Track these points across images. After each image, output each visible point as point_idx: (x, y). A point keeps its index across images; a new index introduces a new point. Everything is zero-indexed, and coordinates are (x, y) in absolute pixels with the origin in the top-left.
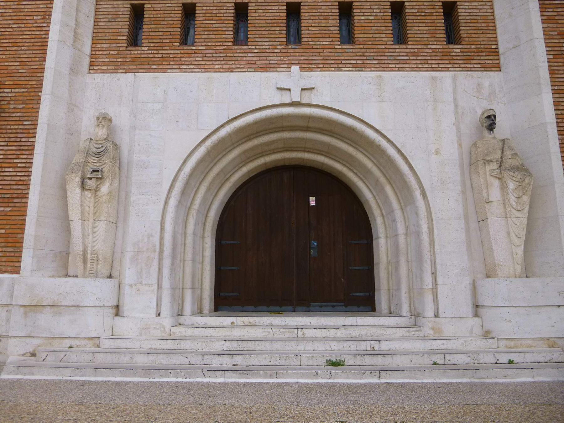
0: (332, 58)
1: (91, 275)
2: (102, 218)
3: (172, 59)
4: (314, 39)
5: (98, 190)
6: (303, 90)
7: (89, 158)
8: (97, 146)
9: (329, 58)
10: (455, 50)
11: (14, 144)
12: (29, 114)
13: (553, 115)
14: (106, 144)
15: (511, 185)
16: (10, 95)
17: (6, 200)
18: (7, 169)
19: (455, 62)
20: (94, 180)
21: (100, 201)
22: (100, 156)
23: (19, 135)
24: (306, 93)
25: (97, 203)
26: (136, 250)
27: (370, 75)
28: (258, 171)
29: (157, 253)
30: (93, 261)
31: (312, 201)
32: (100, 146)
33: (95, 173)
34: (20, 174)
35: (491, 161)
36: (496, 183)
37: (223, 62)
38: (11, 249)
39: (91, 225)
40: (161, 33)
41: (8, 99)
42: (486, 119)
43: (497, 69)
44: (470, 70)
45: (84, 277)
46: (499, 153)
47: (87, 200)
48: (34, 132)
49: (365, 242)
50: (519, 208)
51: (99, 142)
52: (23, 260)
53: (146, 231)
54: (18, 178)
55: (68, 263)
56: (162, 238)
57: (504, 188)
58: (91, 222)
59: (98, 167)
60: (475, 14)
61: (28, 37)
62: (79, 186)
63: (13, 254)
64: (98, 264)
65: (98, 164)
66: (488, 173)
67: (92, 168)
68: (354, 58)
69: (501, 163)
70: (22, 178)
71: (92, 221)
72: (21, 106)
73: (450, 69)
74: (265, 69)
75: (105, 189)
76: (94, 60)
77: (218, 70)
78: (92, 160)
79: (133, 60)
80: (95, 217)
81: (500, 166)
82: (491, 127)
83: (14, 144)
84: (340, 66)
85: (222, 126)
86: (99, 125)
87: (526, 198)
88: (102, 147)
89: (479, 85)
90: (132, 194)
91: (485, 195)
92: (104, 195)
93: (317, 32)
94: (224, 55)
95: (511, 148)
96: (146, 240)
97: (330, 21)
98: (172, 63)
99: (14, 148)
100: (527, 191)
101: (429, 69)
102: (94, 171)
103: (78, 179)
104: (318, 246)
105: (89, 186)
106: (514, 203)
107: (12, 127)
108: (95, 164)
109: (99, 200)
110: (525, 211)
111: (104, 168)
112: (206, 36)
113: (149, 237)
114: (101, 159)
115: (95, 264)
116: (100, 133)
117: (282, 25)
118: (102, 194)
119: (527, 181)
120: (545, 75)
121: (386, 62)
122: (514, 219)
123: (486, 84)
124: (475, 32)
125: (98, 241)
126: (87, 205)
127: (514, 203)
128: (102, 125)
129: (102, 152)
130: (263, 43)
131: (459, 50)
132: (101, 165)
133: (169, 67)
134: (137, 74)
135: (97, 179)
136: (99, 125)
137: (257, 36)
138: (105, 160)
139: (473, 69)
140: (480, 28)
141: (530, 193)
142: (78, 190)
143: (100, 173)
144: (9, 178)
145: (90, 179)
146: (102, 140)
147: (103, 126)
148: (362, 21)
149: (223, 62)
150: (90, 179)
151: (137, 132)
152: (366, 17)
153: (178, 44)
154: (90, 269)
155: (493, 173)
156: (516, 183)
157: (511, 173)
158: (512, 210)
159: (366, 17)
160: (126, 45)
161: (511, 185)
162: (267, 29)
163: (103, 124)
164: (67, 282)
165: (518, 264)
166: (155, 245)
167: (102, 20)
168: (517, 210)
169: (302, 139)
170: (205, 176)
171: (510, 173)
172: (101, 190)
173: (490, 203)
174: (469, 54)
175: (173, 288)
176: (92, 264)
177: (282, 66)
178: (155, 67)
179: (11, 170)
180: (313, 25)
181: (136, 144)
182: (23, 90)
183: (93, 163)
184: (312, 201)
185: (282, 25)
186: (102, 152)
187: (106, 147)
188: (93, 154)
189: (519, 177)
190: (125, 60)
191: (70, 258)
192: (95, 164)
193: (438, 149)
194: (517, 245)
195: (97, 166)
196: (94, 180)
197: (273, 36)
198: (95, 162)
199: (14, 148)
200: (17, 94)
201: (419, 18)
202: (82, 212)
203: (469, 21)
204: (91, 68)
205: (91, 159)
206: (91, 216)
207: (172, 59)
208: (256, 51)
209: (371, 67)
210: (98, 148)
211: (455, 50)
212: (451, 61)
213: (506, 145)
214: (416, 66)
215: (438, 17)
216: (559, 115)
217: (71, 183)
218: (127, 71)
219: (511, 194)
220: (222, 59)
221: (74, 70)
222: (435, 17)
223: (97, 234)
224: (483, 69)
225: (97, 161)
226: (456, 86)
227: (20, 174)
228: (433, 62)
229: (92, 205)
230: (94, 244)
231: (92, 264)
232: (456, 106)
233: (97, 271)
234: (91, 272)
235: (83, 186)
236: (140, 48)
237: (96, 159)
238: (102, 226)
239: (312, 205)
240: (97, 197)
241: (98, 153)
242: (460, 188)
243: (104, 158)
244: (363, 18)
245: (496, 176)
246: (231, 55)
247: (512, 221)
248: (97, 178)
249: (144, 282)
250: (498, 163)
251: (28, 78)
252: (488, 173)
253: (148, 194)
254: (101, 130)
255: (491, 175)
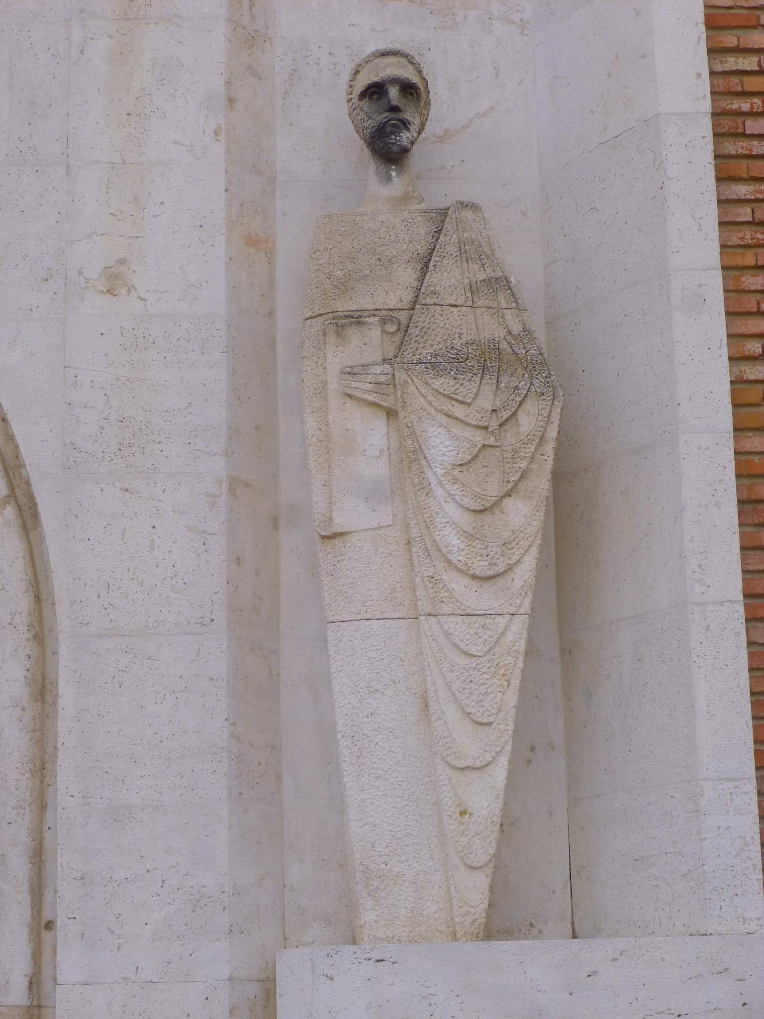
13: (699, 75)
35: (356, 319)
42: (365, 104)
46: (407, 275)
50: (481, 567)
69: (405, 330)
100: (524, 475)
106: (454, 541)
110: (518, 583)
119: (527, 422)
122: (457, 626)
127: (454, 541)
141: (541, 483)
155: (362, 387)
156: (468, 433)
157: (442, 383)
158: (445, 577)
165: (472, 868)
168: (474, 577)
171: (437, 383)
173: (337, 541)
189: (487, 400)
193: (122, 262)
194: (470, 762)
213: (449, 241)
216: (746, 79)
219: (439, 492)
242: (219, 464)
245: (370, 398)
247: (447, 634)
250: (392, 328)
255: (350, 396)
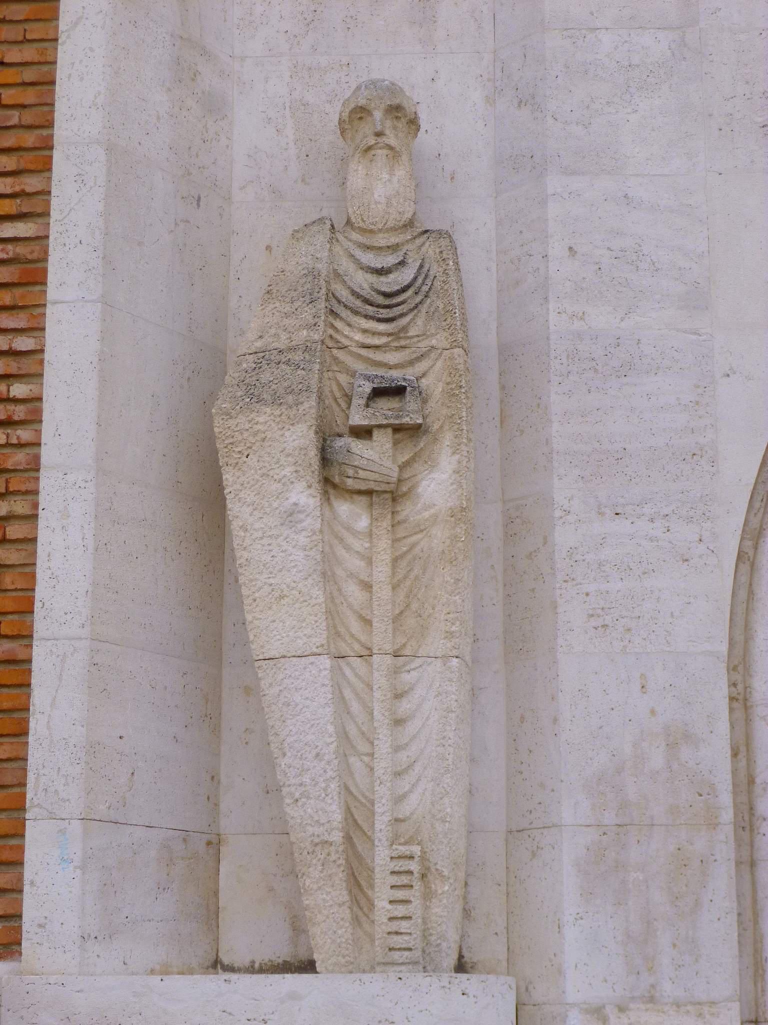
1: (396, 955)
2: (436, 644)
5: (405, 494)
7: (339, 324)
8: (369, 259)
14: (420, 247)
20: (383, 440)
21: (417, 550)
22: (396, 311)
25: (403, 563)
26: (610, 818)
29: (726, 831)
30: (405, 880)
32: (390, 260)
33: (385, 405)
39: (380, 680)
45: (352, 968)
47: (348, 548)
48: (17, 189)
51: (381, 240)
52: (32, 883)
53: (653, 712)
55: (216, 893)
59: (395, 374)
62: (314, 479)
64: (428, 895)
65: (392, 358)
67: (368, 378)
71: (389, 659)
78: (358, 337)
80: (401, 640)
86: (369, 148)
88: (402, 263)
90: (558, 513)
92: (435, 518)
96: (657, 759)
102: (378, 393)
105: (362, 474)
108: (378, 356)
109: (413, 546)
111: (424, 375)
113: (672, 746)
114: (405, 329)
115: (415, 895)
116: (380, 192)
118: (426, 514)
125: (418, 768)
126: (351, 575)
128: (391, 148)
129: (404, 290)
132: (411, 363)
135: (398, 436)
136: (369, 148)
138: (424, 335)
143: (411, 403)
146: (393, 229)
150: (363, 433)
151: (554, 183)
154: (394, 926)
163: (392, 141)
164: (293, 996)
166: (712, 786)
172: (420, 490)
176: (400, 894)
181: (557, 249)
183: (364, 352)
186: (404, 290)
187: (421, 266)
188: (358, 303)
191: (222, 870)
192: (378, 356)
196: (383, 440)
198: (377, 347)
210: (381, 272)
217: (253, 460)
223: (412, 727)
225: (384, 340)
229: (381, 572)
230: (404, 785)
231: (400, 894)
233: (425, 935)
234: (398, 941)
237: (382, 327)
240: (401, 532)
241: (387, 295)
243: (420, 322)
248: (397, 429)
249: (668, 989)
253: (647, 510)
254: (385, 176)
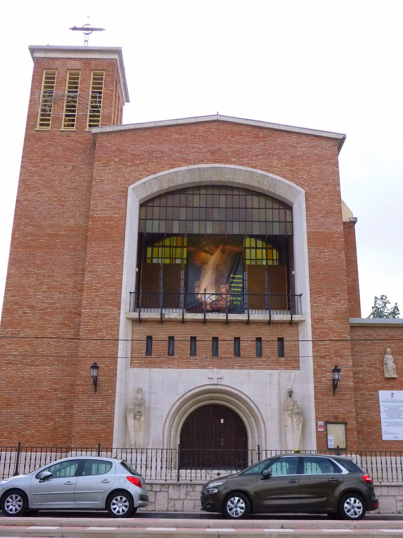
0: (231, 363)
2: (142, 431)
3: (165, 362)
4: (223, 354)
6: (218, 378)
9: (229, 363)
10: (281, 360)
11: (106, 400)
12: (111, 388)
15: (295, 420)
16: (102, 379)
17: (104, 423)
18: (103, 411)
19: (281, 365)
20: (139, 416)
23: (107, 396)
24: (219, 380)
27: (245, 371)
28: (146, 200)
29: (162, 444)
31: (222, 421)
32: (140, 402)
34: (109, 412)
36: (290, 419)
37: (186, 364)
38: (107, 443)
40: (160, 350)
41: (102, 381)
43: (298, 368)
44: (287, 369)
46: (292, 407)
49: (244, 439)
54: (108, 414)
56: (163, 438)
57: (292, 421)
58: (138, 432)
60: (291, 343)
61: (108, 354)
63: (107, 444)
65: (139, 409)
66: (287, 415)
68: (240, 363)
70: (110, 414)
72: (107, 384)
73: (279, 368)
74: (203, 367)
75: (142, 419)
76: (132, 361)
77: (183, 367)
79: (148, 362)
81: (292, 412)
82: (290, 396)
83: (106, 400)
84: (234, 366)
85: (186, 393)
87: (300, 425)
89: (290, 376)
91: (286, 423)
93: (225, 351)
94: (186, 360)
95: (297, 405)
96: (157, 439)
97: (230, 346)
98: (165, 364)
99: (105, 402)
101: (270, 368)
103: (133, 415)
104: (224, 440)
106: (296, 427)
107: (104, 393)
112: (178, 352)
113: (158, 438)
117: (210, 347)
120: (312, 375)
121: (253, 365)
123: (293, 375)
124: (290, 351)
127: (296, 427)
130: (202, 356)
131: (283, 360)
133: (163, 365)
134: (151, 369)
137: (200, 352)
139: (288, 368)
140: (292, 350)
141: (302, 423)
142: (133, 420)
144: (104, 414)
145: (137, 415)
147: (140, 393)
148: (244, 346)
149: (186, 364)
150: (137, 415)
152: (245, 344)
153: (167, 355)
155: (289, 415)
157: (295, 415)
159: (245, 344)
160: (145, 355)
161: (295, 420)
162: (204, 349)
167: (134, 343)
169: (218, 397)
170: (178, 412)
174: (287, 361)
175: (261, 437)
177: (210, 366)
178: (157, 365)
179: (105, 411)
180: (223, 347)
182: (107, 377)
184: (222, 421)
185: (210, 347)
189: (298, 417)
190: (145, 361)
195: (139, 410)
196: (139, 416)
197: (206, 352)
199: (105, 402)
200: (105, 379)
201: (267, 345)
202: (134, 428)
203: (288, 347)
204: (131, 365)
205: (137, 407)
206: (138, 430)
207: (165, 362)
208: (199, 359)
209: (246, 367)
211: (281, 360)
212: (280, 365)
214: (265, 367)
215: (275, 345)
218: (146, 367)
220: (185, 362)
221: (126, 368)
222: (274, 345)
224: (292, 368)
226: (280, 376)
227: (109, 412)
228: (272, 365)
232: (279, 385)
235: (135, 418)
236: (151, 357)
238: (141, 433)
239: (222, 422)
244: (244, 344)
246: (189, 360)
251: (109, 372)
252: (287, 415)
